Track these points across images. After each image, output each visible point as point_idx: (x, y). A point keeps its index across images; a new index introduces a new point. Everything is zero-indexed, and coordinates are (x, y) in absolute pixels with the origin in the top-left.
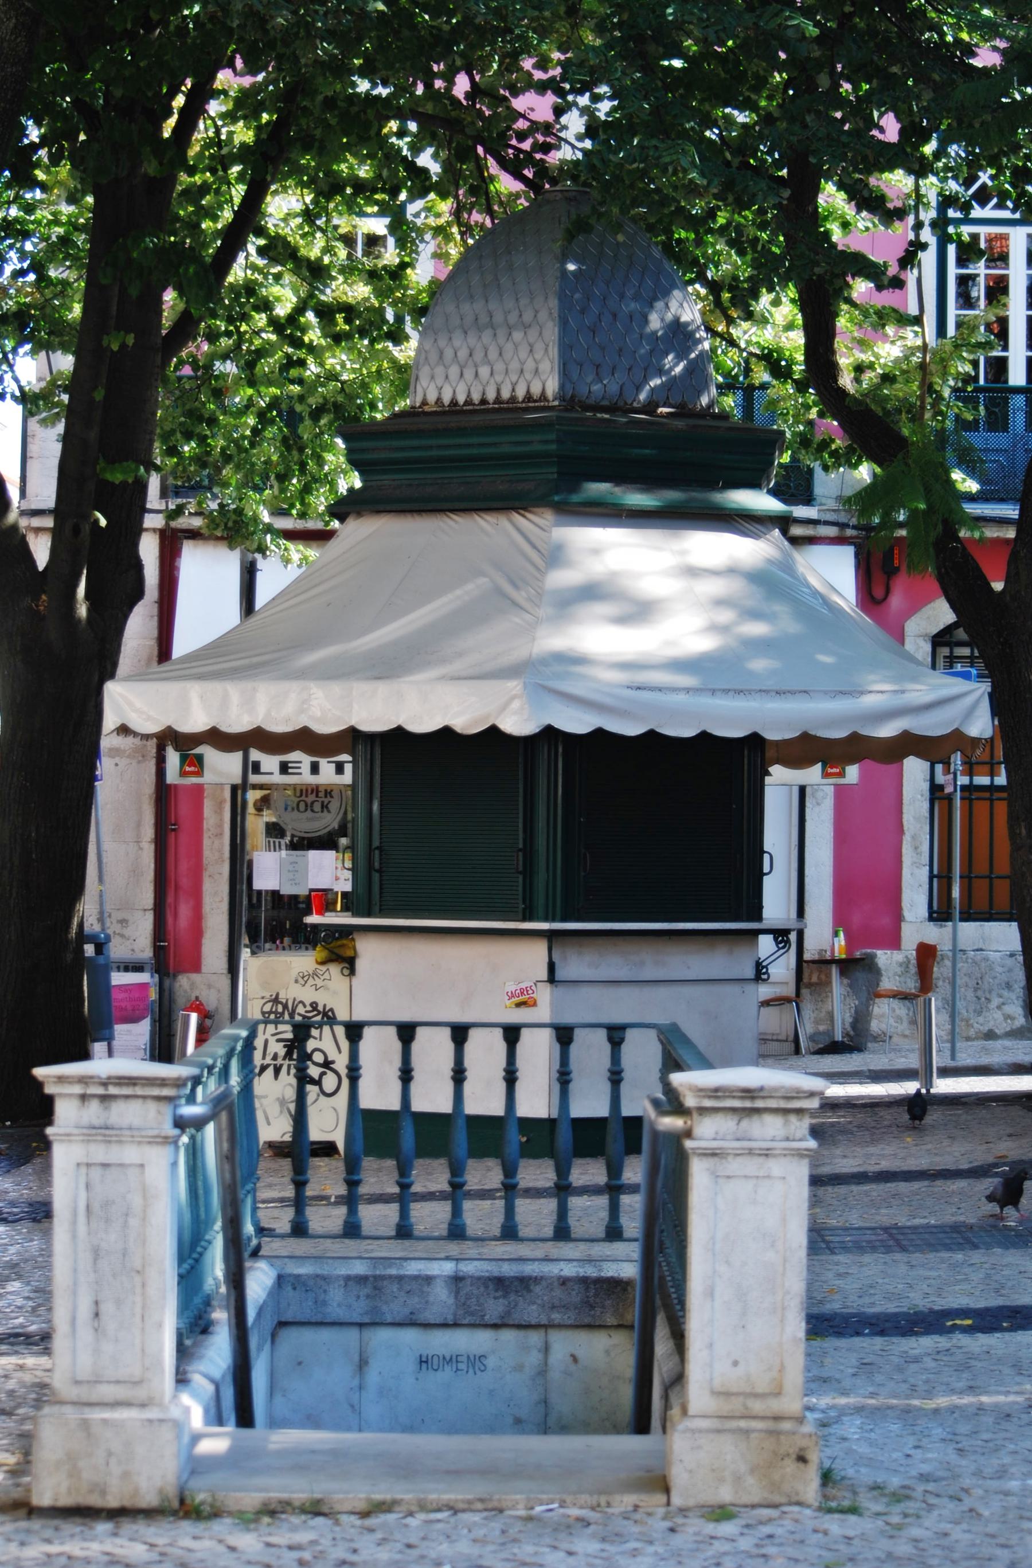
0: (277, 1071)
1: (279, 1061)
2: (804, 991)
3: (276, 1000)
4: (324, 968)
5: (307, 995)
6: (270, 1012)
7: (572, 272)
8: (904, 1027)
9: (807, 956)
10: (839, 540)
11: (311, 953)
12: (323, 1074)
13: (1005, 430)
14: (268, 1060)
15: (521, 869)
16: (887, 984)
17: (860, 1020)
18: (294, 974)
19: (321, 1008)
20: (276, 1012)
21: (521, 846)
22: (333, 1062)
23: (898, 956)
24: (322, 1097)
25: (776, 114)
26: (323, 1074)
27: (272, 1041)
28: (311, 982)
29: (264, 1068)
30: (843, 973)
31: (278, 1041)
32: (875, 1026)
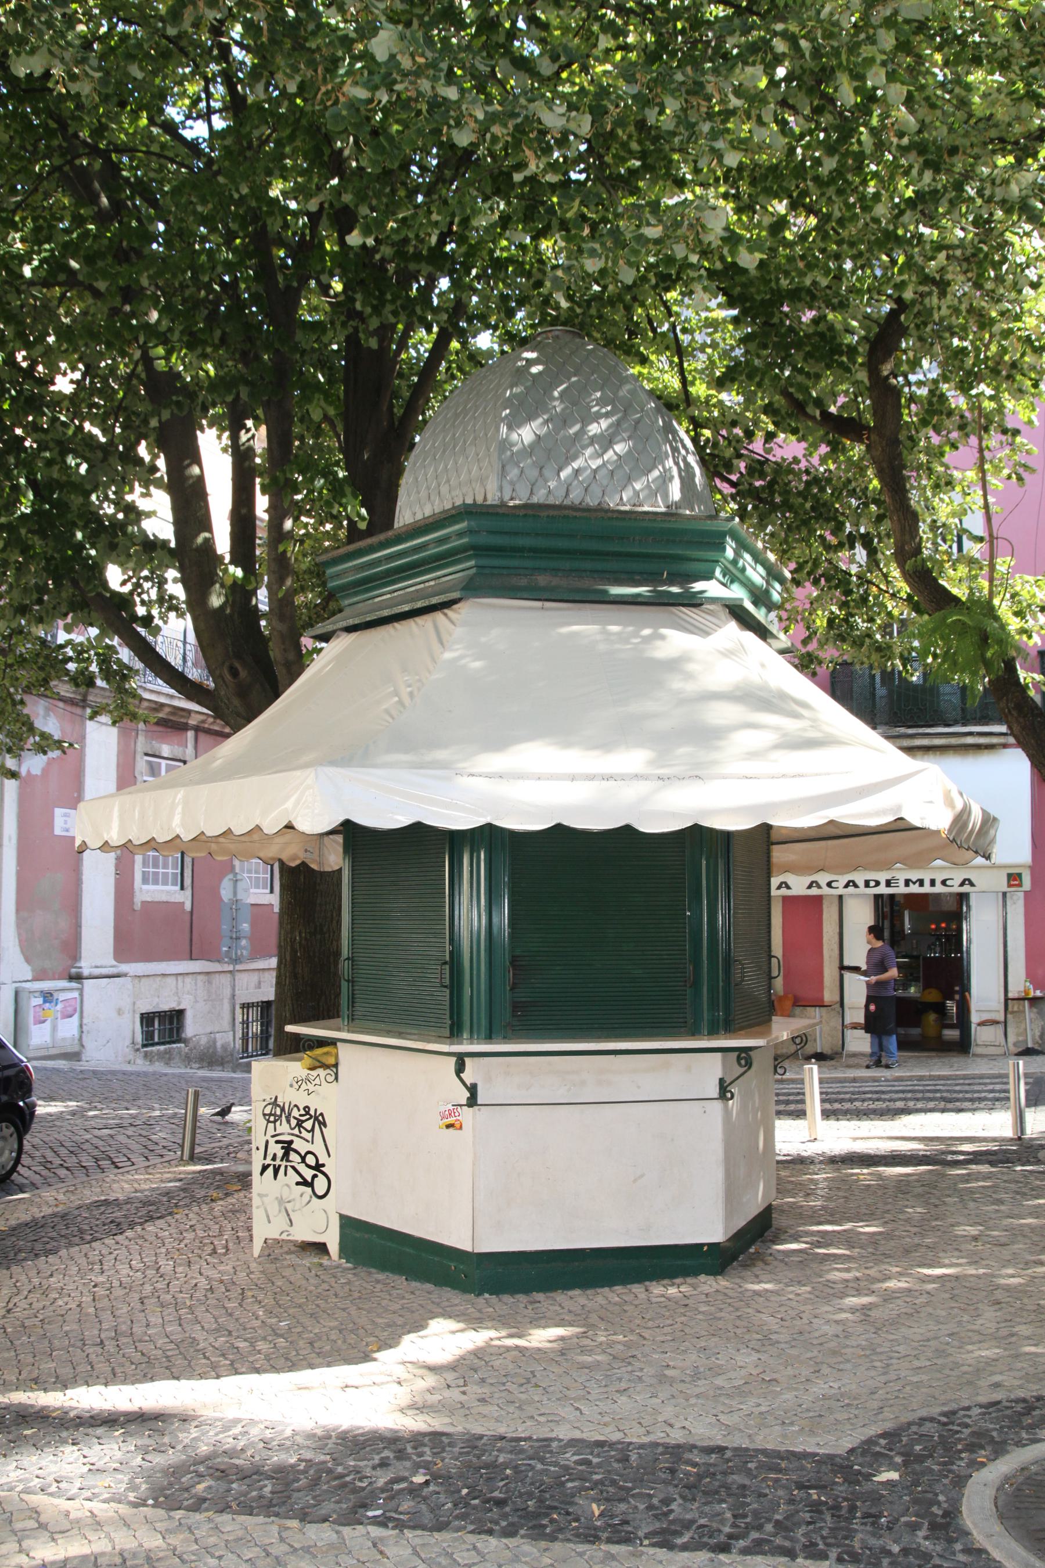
0: (276, 1171)
1: (278, 1162)
2: (1009, 1016)
3: (275, 1103)
4: (314, 1073)
6: (270, 1115)
9: (1010, 995)
11: (300, 1059)
12: (315, 1176)
14: (268, 1161)
15: (447, 982)
18: (290, 1079)
19: (312, 1112)
20: (275, 1115)
21: (448, 958)
22: (323, 1165)
24: (314, 1199)
25: (353, 35)
26: (315, 1176)
27: (272, 1141)
29: (265, 1168)
30: (1031, 1006)
31: (277, 1142)
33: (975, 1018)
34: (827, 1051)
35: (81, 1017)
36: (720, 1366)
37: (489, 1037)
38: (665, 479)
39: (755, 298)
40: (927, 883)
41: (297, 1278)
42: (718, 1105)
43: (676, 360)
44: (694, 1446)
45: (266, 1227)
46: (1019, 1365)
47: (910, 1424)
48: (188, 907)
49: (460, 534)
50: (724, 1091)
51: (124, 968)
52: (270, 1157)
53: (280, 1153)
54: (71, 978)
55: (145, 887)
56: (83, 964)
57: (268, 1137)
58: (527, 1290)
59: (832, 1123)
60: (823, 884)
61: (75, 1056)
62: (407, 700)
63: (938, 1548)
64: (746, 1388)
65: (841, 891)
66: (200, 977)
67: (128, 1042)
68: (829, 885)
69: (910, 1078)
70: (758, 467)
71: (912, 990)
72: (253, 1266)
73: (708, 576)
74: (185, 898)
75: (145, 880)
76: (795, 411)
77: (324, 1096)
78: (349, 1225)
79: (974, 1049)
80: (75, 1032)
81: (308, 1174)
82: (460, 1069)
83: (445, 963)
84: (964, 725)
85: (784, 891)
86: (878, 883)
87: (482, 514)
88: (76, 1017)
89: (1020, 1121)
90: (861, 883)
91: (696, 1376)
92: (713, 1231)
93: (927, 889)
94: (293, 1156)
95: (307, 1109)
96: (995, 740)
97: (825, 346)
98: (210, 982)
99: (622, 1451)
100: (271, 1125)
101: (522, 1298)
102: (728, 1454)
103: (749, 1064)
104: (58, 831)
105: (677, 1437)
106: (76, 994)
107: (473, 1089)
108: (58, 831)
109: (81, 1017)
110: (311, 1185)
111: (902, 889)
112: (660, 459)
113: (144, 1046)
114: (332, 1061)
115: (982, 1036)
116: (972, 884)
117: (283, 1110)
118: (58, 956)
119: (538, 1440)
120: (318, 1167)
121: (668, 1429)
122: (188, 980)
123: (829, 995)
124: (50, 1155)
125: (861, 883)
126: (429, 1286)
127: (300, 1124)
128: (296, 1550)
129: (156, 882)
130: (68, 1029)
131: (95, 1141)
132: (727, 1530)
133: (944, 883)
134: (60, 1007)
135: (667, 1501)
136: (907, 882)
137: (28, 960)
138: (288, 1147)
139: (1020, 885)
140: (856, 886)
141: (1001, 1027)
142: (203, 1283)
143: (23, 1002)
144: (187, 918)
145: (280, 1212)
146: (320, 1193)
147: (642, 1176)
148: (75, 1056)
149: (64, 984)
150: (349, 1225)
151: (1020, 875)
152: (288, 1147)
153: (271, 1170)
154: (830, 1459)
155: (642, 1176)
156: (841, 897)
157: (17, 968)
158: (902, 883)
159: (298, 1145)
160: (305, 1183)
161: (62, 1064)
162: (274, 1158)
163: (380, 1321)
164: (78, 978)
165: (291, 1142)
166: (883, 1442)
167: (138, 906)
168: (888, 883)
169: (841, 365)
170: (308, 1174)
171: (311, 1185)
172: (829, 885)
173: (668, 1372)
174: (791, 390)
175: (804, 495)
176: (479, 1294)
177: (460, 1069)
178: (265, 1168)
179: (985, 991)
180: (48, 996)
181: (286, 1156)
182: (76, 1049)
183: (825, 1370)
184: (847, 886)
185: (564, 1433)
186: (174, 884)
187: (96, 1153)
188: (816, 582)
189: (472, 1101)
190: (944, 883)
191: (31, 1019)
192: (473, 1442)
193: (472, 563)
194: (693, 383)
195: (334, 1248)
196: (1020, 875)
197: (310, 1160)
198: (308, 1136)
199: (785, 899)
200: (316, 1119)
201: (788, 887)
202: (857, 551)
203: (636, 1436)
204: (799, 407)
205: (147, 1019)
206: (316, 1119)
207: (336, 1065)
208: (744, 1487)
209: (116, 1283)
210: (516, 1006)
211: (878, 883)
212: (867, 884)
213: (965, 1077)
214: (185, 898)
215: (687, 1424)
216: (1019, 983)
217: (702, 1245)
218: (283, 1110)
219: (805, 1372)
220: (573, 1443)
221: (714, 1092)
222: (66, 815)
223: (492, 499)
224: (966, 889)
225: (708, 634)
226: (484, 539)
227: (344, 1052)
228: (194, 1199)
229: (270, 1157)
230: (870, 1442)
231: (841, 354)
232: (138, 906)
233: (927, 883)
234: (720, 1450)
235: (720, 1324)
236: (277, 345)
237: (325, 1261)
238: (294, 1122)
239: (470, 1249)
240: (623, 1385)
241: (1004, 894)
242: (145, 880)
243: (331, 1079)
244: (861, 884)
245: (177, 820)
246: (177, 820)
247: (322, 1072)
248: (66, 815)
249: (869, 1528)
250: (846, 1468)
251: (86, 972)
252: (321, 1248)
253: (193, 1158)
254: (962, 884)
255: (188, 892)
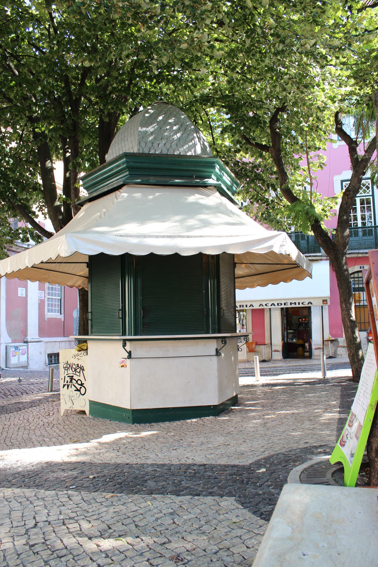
1: (69, 383)
3: (67, 363)
4: (80, 353)
5: (76, 362)
7: (147, 117)
8: (344, 353)
10: (327, 260)
12: (81, 388)
13: (358, 236)
14: (65, 383)
16: (340, 344)
17: (335, 352)
23: (342, 339)
26: (81, 388)
28: (77, 357)
29: (64, 386)
32: (338, 353)
33: (313, 347)
34: (267, 359)
35: (28, 355)
36: (211, 441)
37: (135, 334)
38: (195, 145)
39: (233, 106)
40: (297, 304)
41: (73, 421)
42: (215, 358)
43: (210, 131)
44: (195, 464)
45: (65, 405)
46: (315, 437)
47: (273, 455)
48: (63, 320)
49: (123, 163)
50: (218, 353)
51: (42, 339)
52: (66, 382)
53: (69, 380)
54: (24, 342)
55: (49, 313)
56: (28, 338)
57: (65, 375)
58: (150, 422)
59: (263, 377)
60: (264, 305)
61: (26, 367)
62: (103, 216)
63: (277, 491)
64: (218, 447)
65: (270, 307)
66: (67, 343)
67: (44, 363)
68: (266, 305)
69: (293, 366)
70: (237, 163)
71: (294, 340)
72: (60, 418)
73: (210, 177)
74: (62, 317)
75: (49, 311)
76: (247, 142)
77: (84, 360)
78: (92, 403)
79: (313, 357)
80: (26, 359)
81: (79, 387)
82: (124, 346)
83: (120, 310)
84: (308, 253)
85: (251, 308)
86: (281, 304)
87: (131, 156)
88: (26, 354)
89: (324, 374)
90: (276, 304)
91: (202, 444)
92: (214, 401)
93: (297, 306)
94: (74, 381)
95: (78, 365)
96: (318, 258)
97: (257, 121)
98: (70, 344)
99: (169, 467)
100: (66, 371)
101: (148, 425)
102: (207, 466)
103: (225, 343)
104: (19, 295)
105: (190, 461)
106: (26, 347)
107: (130, 353)
108: (19, 295)
109: (28, 355)
110: (79, 391)
111: (289, 306)
112: (193, 139)
113: (49, 364)
114: (85, 348)
115: (315, 352)
116: (311, 304)
117: (70, 365)
118: (21, 336)
119: (140, 464)
120: (82, 384)
121: (187, 460)
122: (63, 343)
123: (267, 341)
124: (7, 392)
125: (276, 304)
126: (117, 422)
127: (75, 370)
128: (38, 498)
129: (52, 312)
130: (24, 358)
131: (23, 388)
132: (200, 489)
133: (302, 303)
134: (20, 351)
135: (180, 482)
136: (291, 304)
137: (10, 336)
138: (72, 378)
139: (327, 303)
140: (274, 305)
141: (322, 350)
142: (42, 423)
143: (8, 350)
144: (63, 324)
145: (70, 401)
146: (83, 393)
147: (189, 382)
148: (26, 367)
149: (23, 344)
150: (92, 403)
151: (326, 300)
152: (72, 378)
153: (66, 386)
154: (243, 467)
155: (189, 382)
156: (270, 309)
157: (6, 339)
158: (289, 304)
159: (75, 377)
160: (78, 390)
161: (21, 369)
162: (67, 382)
163: (96, 432)
164: (27, 342)
165: (73, 376)
166: (263, 461)
167: (46, 319)
168: (285, 304)
169: (261, 127)
170: (79, 387)
171: (79, 391)
172: (266, 305)
173: (192, 444)
174: (245, 134)
175: (251, 172)
176: (133, 423)
177: (124, 346)
178: (64, 386)
179: (316, 338)
180: (16, 348)
181: (71, 381)
182: (26, 365)
183: (247, 441)
184: (271, 305)
185: (149, 462)
186: (58, 312)
187: (22, 391)
188: (257, 202)
189: (130, 356)
190: (302, 303)
191: (11, 355)
192: (117, 466)
193: (128, 173)
194: (217, 140)
195: (87, 412)
196: (326, 300)
197: (79, 382)
198: (78, 374)
199: (252, 310)
200: (81, 368)
201: (253, 306)
202: (270, 192)
203: (175, 462)
204: (248, 141)
205: (50, 356)
206: (81, 368)
207: (87, 349)
208: (210, 476)
209: (12, 424)
210: (144, 324)
211: (281, 304)
212: (278, 304)
213: (310, 365)
214: (62, 317)
215: (194, 458)
216: (327, 336)
217: (211, 406)
218: (70, 365)
219: (240, 442)
220: (152, 465)
221: (214, 353)
222: (22, 290)
223: (136, 151)
224: (310, 305)
225: (209, 196)
226: (132, 164)
227: (90, 345)
228: (48, 401)
229: (66, 382)
230: (259, 460)
231: (261, 123)
232: (46, 319)
233: (297, 304)
234: (204, 465)
235: (214, 430)
236: (73, 118)
237: (85, 416)
238: (73, 370)
239: (129, 408)
240: (175, 448)
241: (322, 307)
242: (49, 311)
243: (85, 354)
244: (276, 304)
245: (27, 261)
246: (27, 261)
247: (82, 352)
248: (22, 290)
249: (253, 487)
250: (248, 469)
251: (29, 340)
252: (83, 412)
253: (52, 391)
254: (308, 304)
255: (63, 315)
